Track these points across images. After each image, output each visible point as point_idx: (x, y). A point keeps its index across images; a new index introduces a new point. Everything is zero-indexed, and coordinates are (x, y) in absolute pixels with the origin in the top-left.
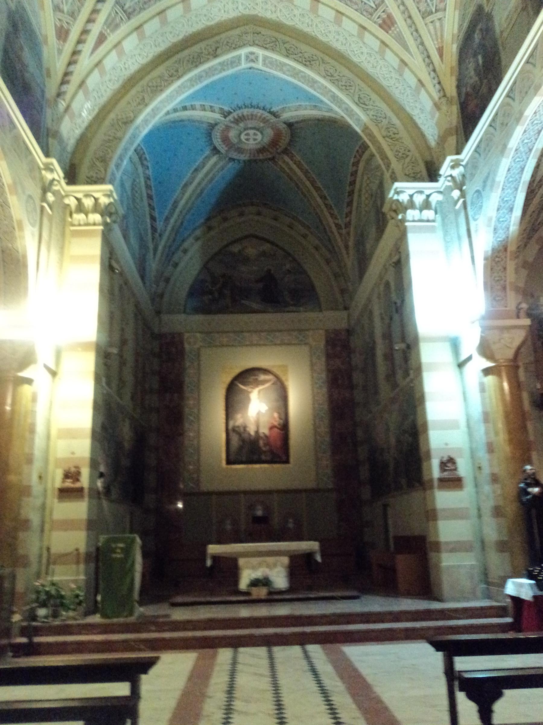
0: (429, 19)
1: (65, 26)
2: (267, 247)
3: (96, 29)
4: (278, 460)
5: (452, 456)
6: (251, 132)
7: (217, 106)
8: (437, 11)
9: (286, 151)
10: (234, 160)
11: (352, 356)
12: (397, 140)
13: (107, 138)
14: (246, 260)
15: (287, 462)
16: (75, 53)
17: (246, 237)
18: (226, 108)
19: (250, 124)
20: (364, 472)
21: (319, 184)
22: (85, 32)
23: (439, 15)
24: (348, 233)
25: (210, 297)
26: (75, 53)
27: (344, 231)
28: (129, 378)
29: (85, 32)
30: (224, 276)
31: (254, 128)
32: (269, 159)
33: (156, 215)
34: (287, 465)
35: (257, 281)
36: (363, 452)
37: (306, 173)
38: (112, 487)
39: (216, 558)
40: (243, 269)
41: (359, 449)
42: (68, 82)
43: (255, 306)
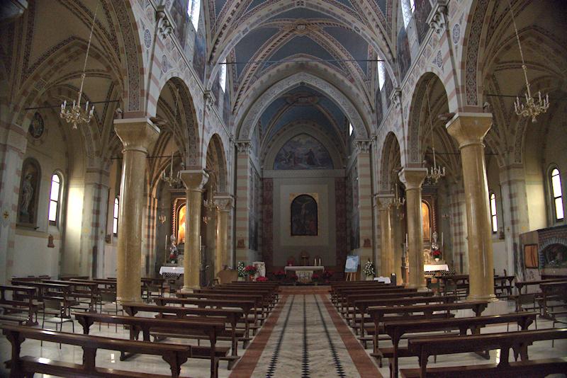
2: (310, 138)
3: (246, 86)
9: (317, 103)
17: (301, 134)
22: (243, 88)
29: (243, 88)
30: (290, 152)
36: (348, 230)
39: (288, 271)
40: (298, 149)
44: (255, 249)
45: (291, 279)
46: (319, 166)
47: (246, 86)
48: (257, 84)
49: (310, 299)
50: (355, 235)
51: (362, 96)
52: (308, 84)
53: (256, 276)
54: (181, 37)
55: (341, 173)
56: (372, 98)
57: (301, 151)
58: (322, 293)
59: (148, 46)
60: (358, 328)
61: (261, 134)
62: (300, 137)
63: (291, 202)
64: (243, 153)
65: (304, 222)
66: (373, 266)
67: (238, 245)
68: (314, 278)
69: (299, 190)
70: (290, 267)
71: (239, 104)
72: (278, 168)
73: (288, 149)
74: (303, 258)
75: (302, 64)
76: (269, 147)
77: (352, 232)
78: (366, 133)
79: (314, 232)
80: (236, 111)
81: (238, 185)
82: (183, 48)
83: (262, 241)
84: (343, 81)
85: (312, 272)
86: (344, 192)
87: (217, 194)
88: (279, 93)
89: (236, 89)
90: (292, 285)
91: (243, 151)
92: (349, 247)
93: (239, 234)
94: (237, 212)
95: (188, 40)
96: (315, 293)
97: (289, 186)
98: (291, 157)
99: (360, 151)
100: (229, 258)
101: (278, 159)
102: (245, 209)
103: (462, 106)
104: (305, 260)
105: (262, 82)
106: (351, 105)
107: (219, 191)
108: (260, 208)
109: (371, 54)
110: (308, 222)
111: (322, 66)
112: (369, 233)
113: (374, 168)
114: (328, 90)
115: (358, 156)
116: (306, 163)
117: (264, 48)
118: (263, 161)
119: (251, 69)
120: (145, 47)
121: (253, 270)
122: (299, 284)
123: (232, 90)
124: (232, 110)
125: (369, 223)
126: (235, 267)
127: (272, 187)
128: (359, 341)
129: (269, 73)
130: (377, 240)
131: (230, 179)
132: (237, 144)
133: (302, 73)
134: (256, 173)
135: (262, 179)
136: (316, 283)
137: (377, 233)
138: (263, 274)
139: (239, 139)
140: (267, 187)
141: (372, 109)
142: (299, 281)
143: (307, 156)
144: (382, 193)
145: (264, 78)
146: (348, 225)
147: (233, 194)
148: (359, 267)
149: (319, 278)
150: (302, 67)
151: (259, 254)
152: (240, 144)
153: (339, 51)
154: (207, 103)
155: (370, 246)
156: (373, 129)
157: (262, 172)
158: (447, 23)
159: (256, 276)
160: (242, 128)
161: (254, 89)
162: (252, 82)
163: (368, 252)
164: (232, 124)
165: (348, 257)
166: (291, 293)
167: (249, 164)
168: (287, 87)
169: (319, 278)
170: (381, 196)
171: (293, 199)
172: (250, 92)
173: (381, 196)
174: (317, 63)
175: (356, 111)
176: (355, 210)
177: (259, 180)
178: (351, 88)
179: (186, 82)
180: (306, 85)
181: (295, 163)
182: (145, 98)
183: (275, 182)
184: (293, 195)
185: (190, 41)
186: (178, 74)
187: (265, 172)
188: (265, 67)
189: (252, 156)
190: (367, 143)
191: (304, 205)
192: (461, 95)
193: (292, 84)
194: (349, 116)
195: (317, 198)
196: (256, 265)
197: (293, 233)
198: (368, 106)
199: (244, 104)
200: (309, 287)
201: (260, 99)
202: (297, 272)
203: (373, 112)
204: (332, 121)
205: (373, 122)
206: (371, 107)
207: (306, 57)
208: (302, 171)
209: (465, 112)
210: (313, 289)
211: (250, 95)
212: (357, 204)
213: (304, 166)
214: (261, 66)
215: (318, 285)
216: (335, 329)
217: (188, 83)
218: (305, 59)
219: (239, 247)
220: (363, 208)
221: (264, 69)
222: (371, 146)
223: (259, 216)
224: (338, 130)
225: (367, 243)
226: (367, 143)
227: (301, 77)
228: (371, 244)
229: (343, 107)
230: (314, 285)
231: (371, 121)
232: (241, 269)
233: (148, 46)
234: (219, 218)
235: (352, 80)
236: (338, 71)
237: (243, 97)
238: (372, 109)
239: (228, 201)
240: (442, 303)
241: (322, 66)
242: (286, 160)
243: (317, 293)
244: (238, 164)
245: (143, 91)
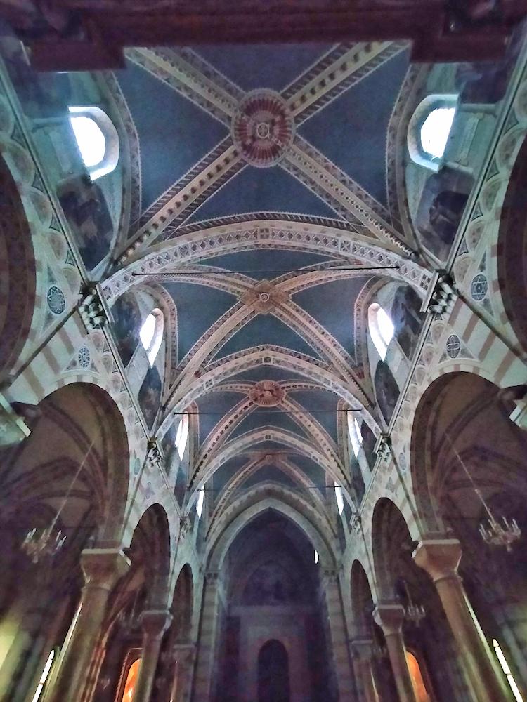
3: (220, 511)
16: (214, 520)
29: (217, 513)
47: (220, 511)
51: (324, 521)
54: (167, 464)
56: (334, 523)
57: (270, 582)
71: (212, 530)
80: (209, 538)
107: (100, 539)
114: (293, 516)
150: (269, 493)
152: (209, 575)
154: (182, 531)
162: (226, 508)
188: (238, 493)
190: (333, 573)
194: (314, 542)
198: (330, 531)
206: (333, 531)
235: (314, 506)
237: (216, 522)
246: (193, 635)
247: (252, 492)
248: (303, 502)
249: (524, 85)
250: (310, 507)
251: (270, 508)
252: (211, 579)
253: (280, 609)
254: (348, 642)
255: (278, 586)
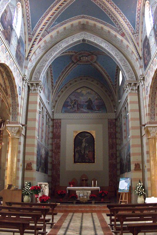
0: (135, 35)
1: (31, 38)
2: (89, 90)
3: (39, 38)
4: (91, 162)
5: (139, 163)
6: (84, 57)
7: (73, 51)
8: (136, 33)
9: (95, 62)
10: (79, 64)
11: (117, 128)
12: (127, 67)
13: (40, 66)
14: (82, 95)
15: (94, 162)
16: (33, 44)
17: (83, 87)
18: (76, 51)
19: (84, 55)
20: (118, 166)
21: (106, 72)
22: (36, 39)
23: (137, 34)
24: (116, 87)
25: (70, 107)
26: (33, 44)
27: (115, 87)
28: (44, 135)
29: (36, 39)
30: (74, 100)
31: (85, 56)
32: (90, 64)
33: (53, 81)
34: (94, 164)
35: (86, 102)
36: (118, 160)
37: (102, 68)
38: (39, 169)
39: (69, 190)
40: (81, 98)
41: (117, 158)
42: (31, 53)
43: (85, 110)
44: (45, 171)
45: (72, 198)
46: (96, 110)
47: (39, 38)
48: (47, 38)
49: (87, 217)
50: (125, 162)
51: (131, 48)
52: (88, 41)
53: (40, 195)
54: (8, 38)
55: (112, 116)
56: (140, 48)
57: (82, 99)
58: (99, 212)
59: (20, 95)
60: (113, 225)
61: (52, 86)
62: (82, 89)
63: (74, 137)
64: (35, 92)
65: (84, 153)
66: (143, 187)
67: (27, 167)
68: (91, 197)
69: (80, 128)
70: (72, 188)
71: (32, 52)
72: (66, 112)
73: (73, 98)
74: (83, 180)
75: (83, 24)
76: (59, 96)
77: (121, 160)
78: (135, 77)
79: (92, 160)
80: (30, 57)
81: (28, 117)
82: (9, 46)
83: (49, 164)
84: (116, 36)
85: (90, 192)
86: (115, 130)
87: (10, 123)
88: (65, 46)
89: (30, 40)
90: (72, 203)
91: (35, 90)
92: (119, 172)
93: (27, 158)
94: (27, 139)
95: (13, 41)
96: (92, 212)
97: (73, 126)
98: (75, 103)
99: (130, 91)
100: (17, 178)
101: (65, 105)
102: (34, 137)
103: (148, 121)
104: (84, 182)
105: (51, 37)
106: (122, 55)
107: (11, 121)
108: (50, 141)
109: (139, 10)
110: (87, 152)
111: (99, 25)
112: (139, 158)
113: (142, 104)
114: (104, 45)
115: (129, 96)
116: (86, 108)
117: (53, 7)
118: (54, 107)
119: (43, 24)
120: (19, 95)
121: (37, 190)
122: (79, 202)
123: (27, 40)
124: (26, 57)
125: (138, 150)
126: (23, 186)
127: (60, 126)
128: (109, 226)
129: (57, 30)
130: (146, 164)
131: (21, 110)
132: (29, 84)
133: (83, 32)
134: (47, 112)
135: (53, 120)
136: (93, 202)
137: (146, 157)
138: (47, 193)
139: (33, 80)
140: (56, 126)
141: (139, 56)
142: (78, 199)
143: (87, 103)
144: (150, 123)
145: (54, 33)
146: (118, 155)
147: (24, 123)
148: (131, 188)
149: (96, 198)
150: (84, 28)
151: (49, 176)
152: (32, 84)
153: (113, 10)
154: (24, 83)
155: (140, 170)
156: (140, 72)
157: (53, 114)
158: (144, 84)
159: (40, 195)
160: (35, 71)
161: (45, 42)
162: (44, 36)
163: (139, 175)
164: (26, 67)
165: (121, 179)
166: (70, 211)
167: (39, 101)
168: (72, 42)
169: (96, 198)
170: (150, 125)
171: (76, 135)
172: (42, 43)
173: (150, 125)
174: (96, 23)
175: (126, 61)
176: (125, 142)
177: (50, 120)
178: (122, 41)
179: (10, 67)
180: (86, 42)
181: (78, 108)
182: (19, 116)
183: (62, 121)
184: (76, 132)
185: (14, 42)
186: (5, 61)
187: (55, 115)
188: (54, 25)
189: (42, 95)
190: (135, 84)
191: (84, 140)
192: (148, 116)
193: (76, 40)
194: (121, 64)
195: (94, 135)
196: (40, 185)
197: (76, 161)
198: (136, 55)
199: (36, 52)
200: (87, 205)
201: (50, 51)
202: (77, 192)
203: (140, 58)
204: (105, 76)
205: (141, 67)
206: (139, 54)
207: (87, 18)
208: (82, 115)
209: (149, 124)
210: (91, 207)
211: (41, 46)
212: (127, 134)
213: (85, 110)
214: (51, 22)
215: (95, 203)
216: (102, 232)
217: (12, 68)
218: (86, 20)
219: (27, 169)
220: (133, 137)
221: (53, 26)
222: (138, 87)
223: (50, 147)
224: (110, 83)
225: (138, 167)
226: (135, 84)
227: (83, 35)
228: (141, 168)
229: (115, 57)
230: (91, 203)
231: (139, 66)
232: (28, 188)
233: (20, 95)
234: (10, 143)
235: (123, 35)
236: (112, 28)
237: (36, 46)
238: (139, 56)
239: (18, 128)
240: (152, 206)
241: (99, 25)
242: (71, 106)
243: (95, 211)
244: (30, 100)
245: (18, 113)
246: (21, 120)
247: (68, 25)
248: (113, 33)
249: (156, 59)
250: (119, 37)
251: (84, 40)
252: (33, 87)
253: (90, 115)
254: (141, 125)
255: (90, 102)
